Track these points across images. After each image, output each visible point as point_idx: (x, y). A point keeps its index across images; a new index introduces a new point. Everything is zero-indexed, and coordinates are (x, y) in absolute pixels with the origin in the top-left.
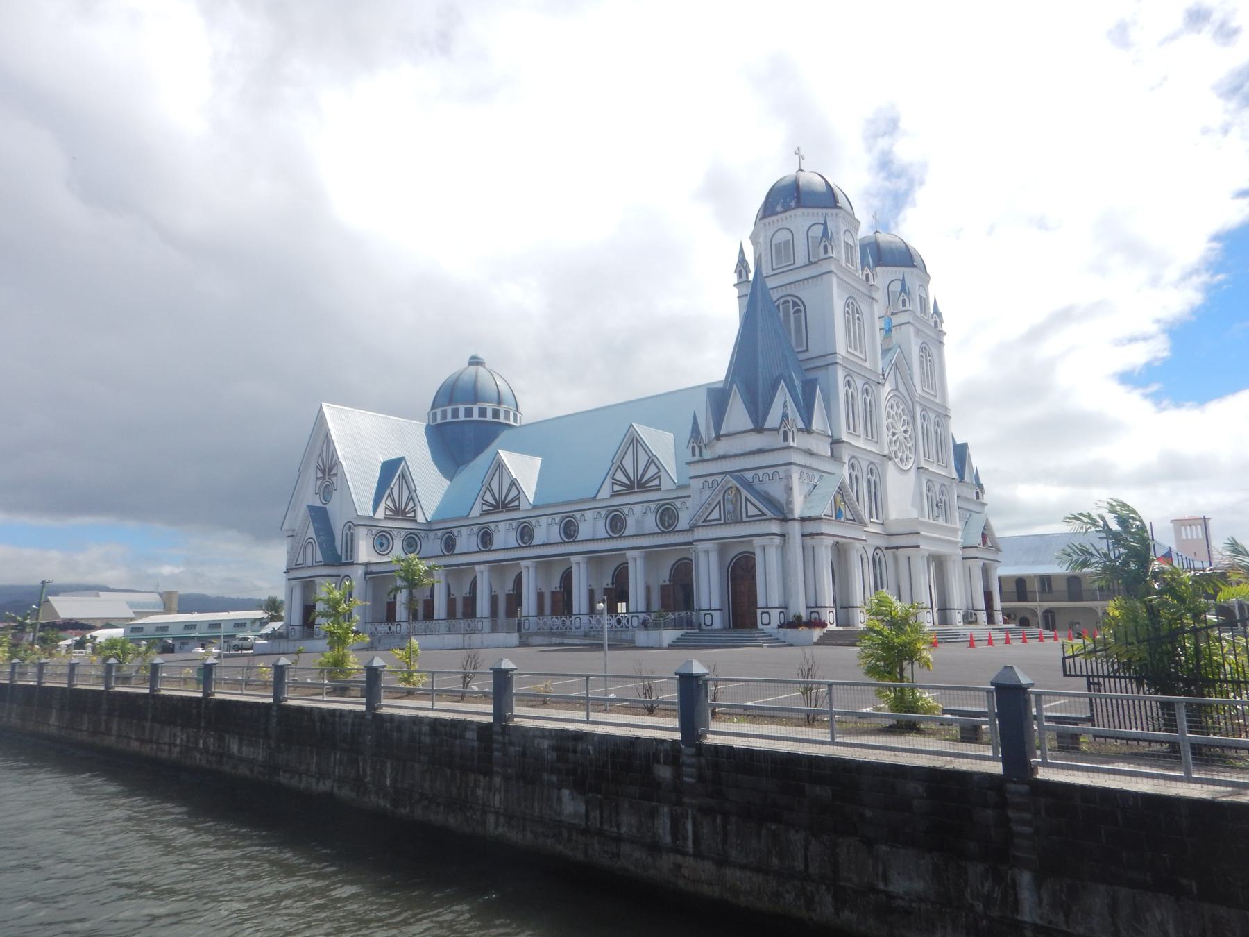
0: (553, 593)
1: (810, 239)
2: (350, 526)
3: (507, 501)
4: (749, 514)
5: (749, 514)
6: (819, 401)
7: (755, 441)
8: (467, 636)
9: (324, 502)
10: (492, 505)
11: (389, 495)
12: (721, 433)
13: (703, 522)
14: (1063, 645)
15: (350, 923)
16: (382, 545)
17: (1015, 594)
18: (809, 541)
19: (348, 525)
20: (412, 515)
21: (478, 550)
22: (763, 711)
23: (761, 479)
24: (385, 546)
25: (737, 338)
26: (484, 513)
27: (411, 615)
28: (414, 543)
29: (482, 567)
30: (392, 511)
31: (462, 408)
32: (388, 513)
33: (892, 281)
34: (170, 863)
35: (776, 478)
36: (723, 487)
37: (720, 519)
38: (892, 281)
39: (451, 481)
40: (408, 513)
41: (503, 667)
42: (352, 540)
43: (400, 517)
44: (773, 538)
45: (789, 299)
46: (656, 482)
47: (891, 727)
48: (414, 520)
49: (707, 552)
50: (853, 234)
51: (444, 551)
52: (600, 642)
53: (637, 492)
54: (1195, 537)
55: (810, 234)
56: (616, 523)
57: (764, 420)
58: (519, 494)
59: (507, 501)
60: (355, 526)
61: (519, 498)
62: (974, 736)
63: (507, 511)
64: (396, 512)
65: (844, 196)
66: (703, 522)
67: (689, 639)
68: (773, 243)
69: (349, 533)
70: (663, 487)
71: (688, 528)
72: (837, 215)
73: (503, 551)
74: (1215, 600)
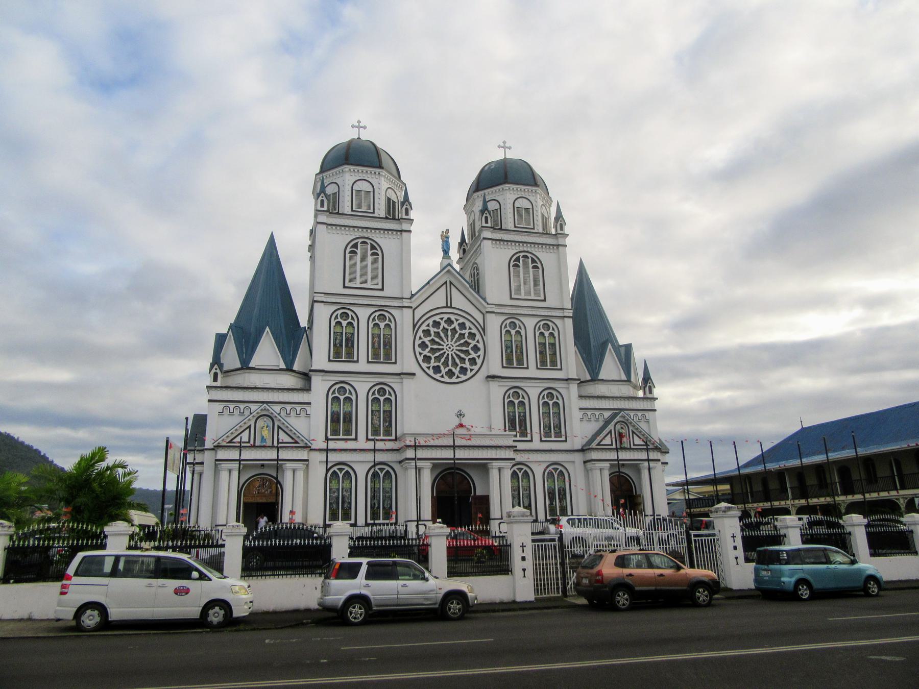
1: (354, 192)
4: (248, 441)
6: (304, 341)
7: (626, 390)
12: (250, 366)
13: (597, 445)
18: (589, 465)
23: (597, 417)
25: (601, 306)
35: (303, 414)
36: (258, 413)
37: (634, 445)
44: (595, 464)
49: (230, 471)
50: (397, 192)
55: (355, 187)
57: (598, 373)
66: (597, 445)
71: (212, 447)
72: (379, 173)
73: (391, 452)
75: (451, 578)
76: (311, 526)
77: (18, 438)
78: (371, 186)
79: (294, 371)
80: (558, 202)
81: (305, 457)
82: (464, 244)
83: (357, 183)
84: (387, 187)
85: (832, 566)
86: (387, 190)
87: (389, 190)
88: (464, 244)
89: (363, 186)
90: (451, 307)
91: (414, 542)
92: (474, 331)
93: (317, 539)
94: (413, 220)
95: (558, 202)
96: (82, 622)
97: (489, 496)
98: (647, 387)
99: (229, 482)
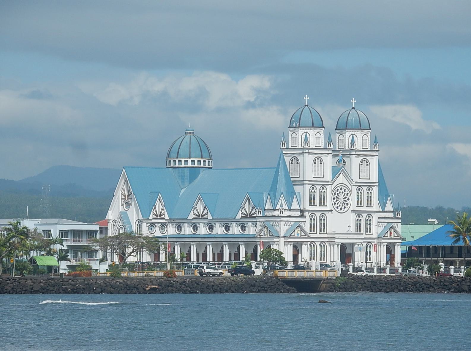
0: (218, 253)
3: (251, 214)
8: (164, 251)
9: (126, 209)
10: (245, 214)
11: (154, 209)
16: (151, 229)
20: (163, 216)
21: (316, 243)
22: (161, 251)
24: (153, 230)
26: (194, 218)
28: (164, 228)
29: (193, 243)
30: (155, 215)
31: (183, 161)
32: (154, 216)
40: (162, 215)
42: (324, 198)
43: (159, 218)
45: (319, 158)
46: (207, 216)
48: (164, 219)
51: (241, 231)
53: (159, 218)
56: (243, 228)
58: (208, 212)
59: (251, 214)
60: (141, 222)
61: (208, 214)
63: (203, 218)
64: (157, 216)
65: (367, 120)
69: (139, 224)
70: (209, 218)
74: (239, 261)
80: (376, 137)
81: (278, 240)
90: (342, 184)
92: (348, 192)
95: (376, 137)
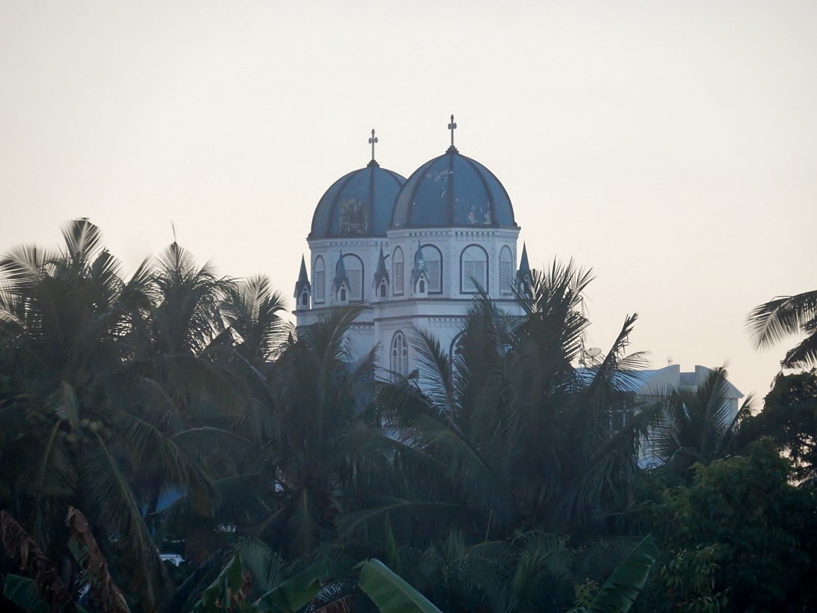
1: (463, 264)
2: (400, 336)
4: (463, 291)
5: (463, 291)
14: (471, 278)
15: (468, 383)
17: (405, 180)
19: (397, 336)
27: (459, 338)
33: (485, 251)
34: (801, 320)
38: (485, 251)
39: (737, 399)
41: (126, 281)
47: (382, 255)
52: (92, 225)
54: (594, 377)
62: (642, 406)
67: (570, 347)
68: (463, 260)
75: (386, 293)
76: (511, 241)
77: (762, 410)
78: (484, 254)
79: (403, 261)
82: (306, 287)
83: (466, 250)
84: (502, 246)
85: (415, 346)
86: (502, 249)
87: (320, 259)
88: (306, 287)
89: (475, 254)
91: (507, 240)
93: (185, 277)
94: (520, 228)
96: (774, 385)
97: (382, 296)
98: (418, 284)
99: (174, 232)
